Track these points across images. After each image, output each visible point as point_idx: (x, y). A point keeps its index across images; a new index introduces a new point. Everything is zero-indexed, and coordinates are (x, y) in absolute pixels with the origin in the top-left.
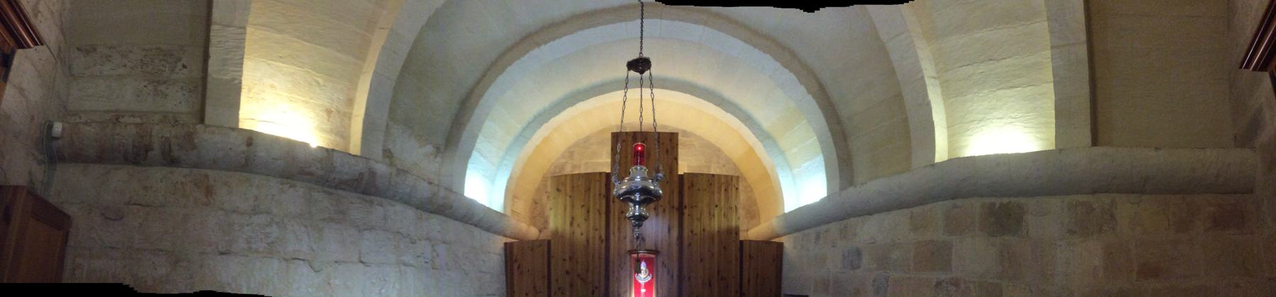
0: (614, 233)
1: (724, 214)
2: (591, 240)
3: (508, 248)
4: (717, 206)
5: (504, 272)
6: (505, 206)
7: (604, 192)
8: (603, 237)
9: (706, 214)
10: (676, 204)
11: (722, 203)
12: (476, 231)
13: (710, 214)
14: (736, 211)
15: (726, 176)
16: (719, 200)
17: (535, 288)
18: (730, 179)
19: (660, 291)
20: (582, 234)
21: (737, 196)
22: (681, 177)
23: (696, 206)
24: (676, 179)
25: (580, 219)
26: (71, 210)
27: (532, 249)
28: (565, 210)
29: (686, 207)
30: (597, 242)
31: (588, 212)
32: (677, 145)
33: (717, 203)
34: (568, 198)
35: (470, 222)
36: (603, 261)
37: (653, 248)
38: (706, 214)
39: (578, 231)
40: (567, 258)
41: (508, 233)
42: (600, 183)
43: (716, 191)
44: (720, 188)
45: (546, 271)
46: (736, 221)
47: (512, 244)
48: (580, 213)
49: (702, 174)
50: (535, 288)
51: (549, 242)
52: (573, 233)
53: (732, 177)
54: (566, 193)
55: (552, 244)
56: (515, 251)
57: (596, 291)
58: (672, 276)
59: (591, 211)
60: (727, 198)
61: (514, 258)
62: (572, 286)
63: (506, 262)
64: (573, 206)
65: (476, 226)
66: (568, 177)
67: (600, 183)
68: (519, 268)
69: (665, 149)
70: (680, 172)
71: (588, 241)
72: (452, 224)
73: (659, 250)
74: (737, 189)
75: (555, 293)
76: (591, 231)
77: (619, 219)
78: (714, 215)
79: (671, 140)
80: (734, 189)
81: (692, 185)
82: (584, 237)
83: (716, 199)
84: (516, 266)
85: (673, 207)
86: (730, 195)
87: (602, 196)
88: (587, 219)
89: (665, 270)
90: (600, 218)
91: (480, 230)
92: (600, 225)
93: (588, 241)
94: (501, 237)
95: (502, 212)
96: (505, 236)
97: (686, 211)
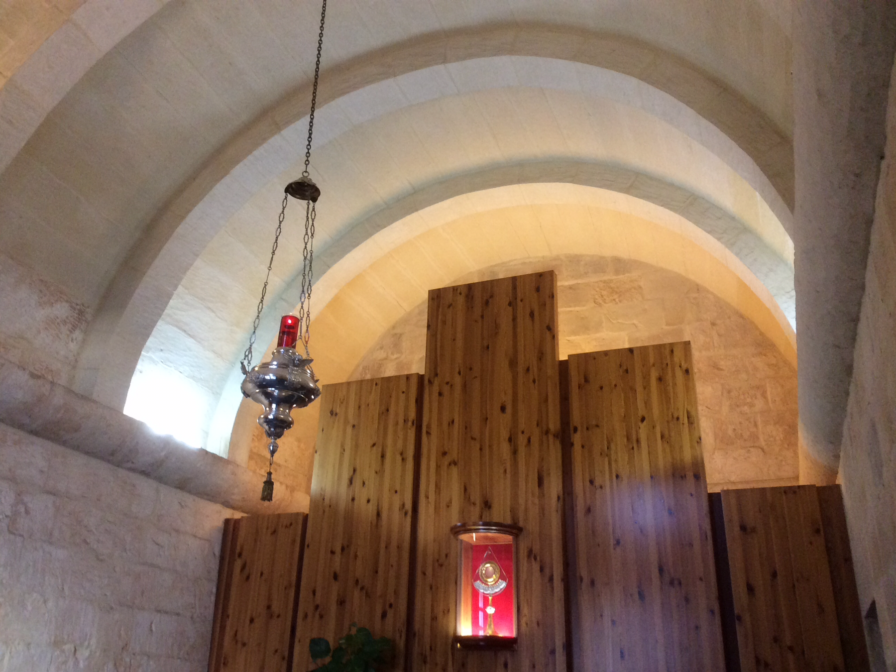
0: (427, 497)
1: (662, 437)
2: (384, 515)
3: (230, 528)
4: (643, 419)
5: (214, 575)
6: (233, 444)
7: (412, 415)
8: (409, 506)
9: (620, 441)
10: (554, 424)
11: (656, 411)
12: (146, 487)
13: (628, 438)
14: (691, 423)
15: (659, 348)
16: (647, 403)
17: (269, 607)
18: (667, 352)
19: (525, 610)
20: (368, 501)
21: (689, 388)
22: (564, 365)
23: (597, 426)
24: (552, 372)
25: (367, 473)
26: (502, 666)
27: (274, 532)
28: (342, 454)
29: (575, 430)
30: (397, 516)
31: (383, 456)
32: (552, 296)
33: (642, 411)
34: (349, 429)
35: (129, 465)
36: (406, 555)
37: (509, 521)
38: (620, 441)
39: (362, 495)
40: (338, 550)
41: (236, 498)
42: (407, 399)
43: (639, 389)
44: (646, 377)
45: (294, 574)
46: (692, 447)
47: (237, 522)
48: (368, 460)
49: (606, 353)
50: (269, 607)
51: (306, 517)
52: (353, 499)
53: (671, 348)
54: (346, 422)
55: (310, 524)
56: (242, 533)
57: (390, 614)
58: (551, 579)
59: (388, 455)
60: (666, 397)
61: (238, 550)
62: (341, 603)
63: (222, 558)
64: (356, 446)
65: (145, 473)
66: (353, 389)
67: (407, 399)
68: (243, 568)
69: (528, 312)
70: (563, 356)
71: (378, 515)
72: (77, 463)
73: (521, 524)
74: (687, 371)
75: (306, 616)
76: (386, 495)
77: (438, 467)
78: (638, 441)
79: (538, 290)
80: (679, 374)
81: (586, 380)
82: (371, 509)
83: (640, 404)
84: (238, 564)
85: (547, 432)
86: (670, 388)
87: (586, 581)
88: (380, 473)
89: (536, 567)
90: (404, 471)
91: (154, 484)
92: (402, 483)
93: (378, 515)
94: (218, 507)
95: (225, 456)
96: (227, 504)
97: (577, 439)
